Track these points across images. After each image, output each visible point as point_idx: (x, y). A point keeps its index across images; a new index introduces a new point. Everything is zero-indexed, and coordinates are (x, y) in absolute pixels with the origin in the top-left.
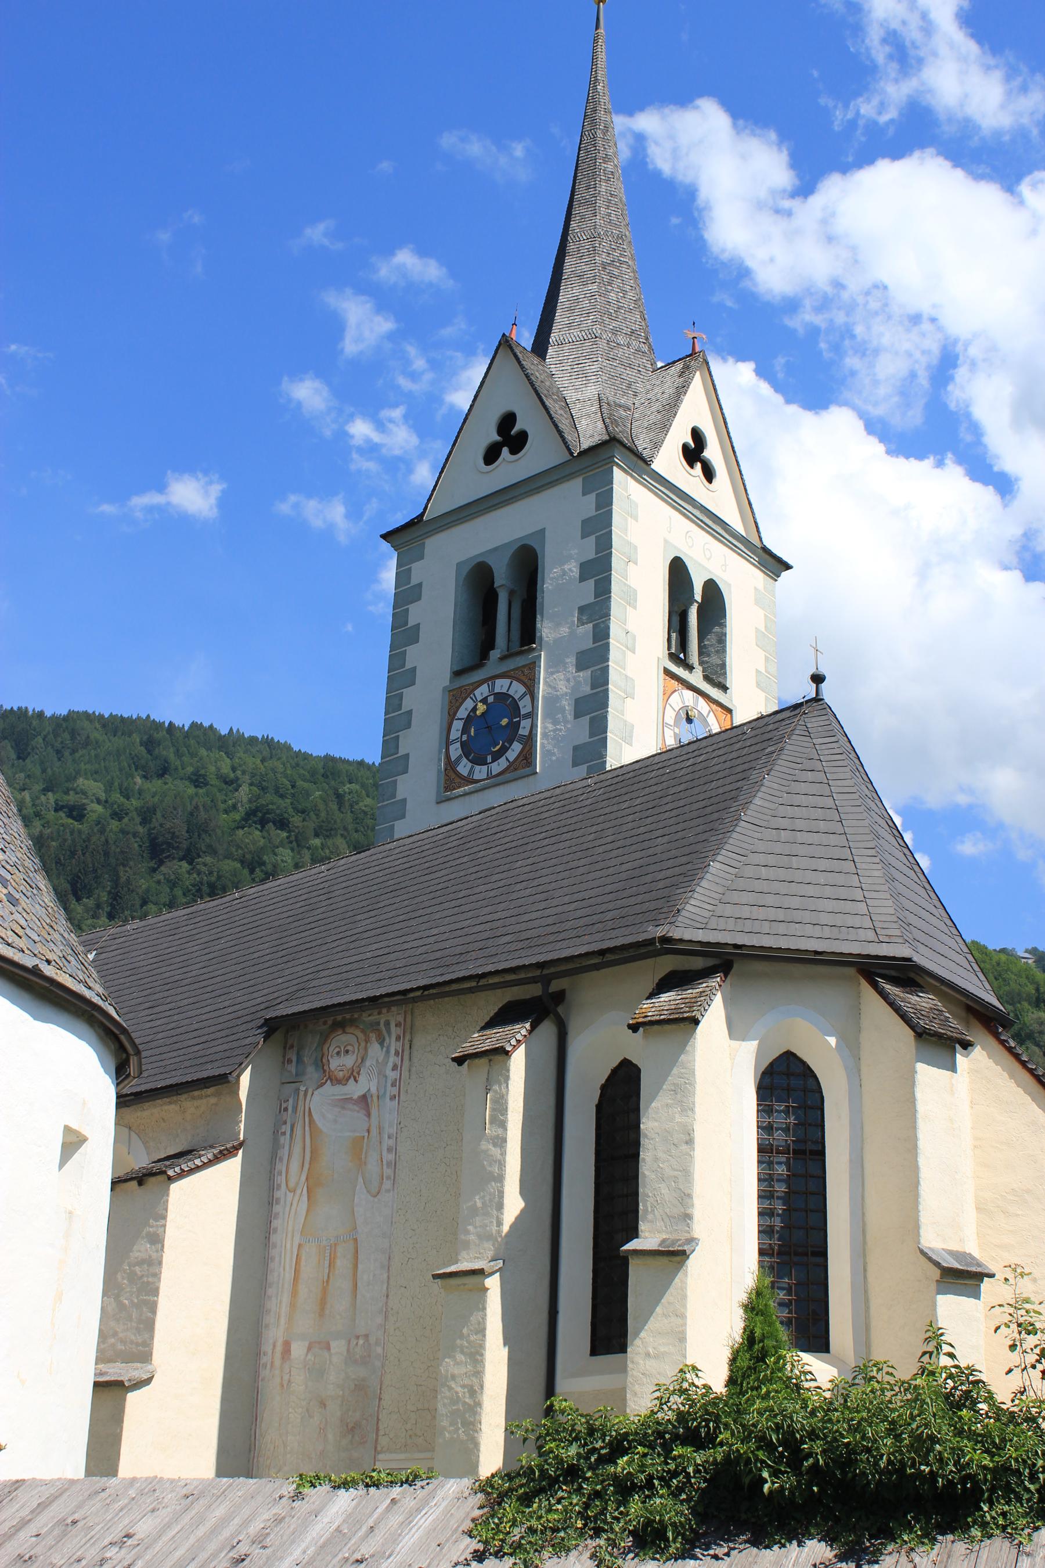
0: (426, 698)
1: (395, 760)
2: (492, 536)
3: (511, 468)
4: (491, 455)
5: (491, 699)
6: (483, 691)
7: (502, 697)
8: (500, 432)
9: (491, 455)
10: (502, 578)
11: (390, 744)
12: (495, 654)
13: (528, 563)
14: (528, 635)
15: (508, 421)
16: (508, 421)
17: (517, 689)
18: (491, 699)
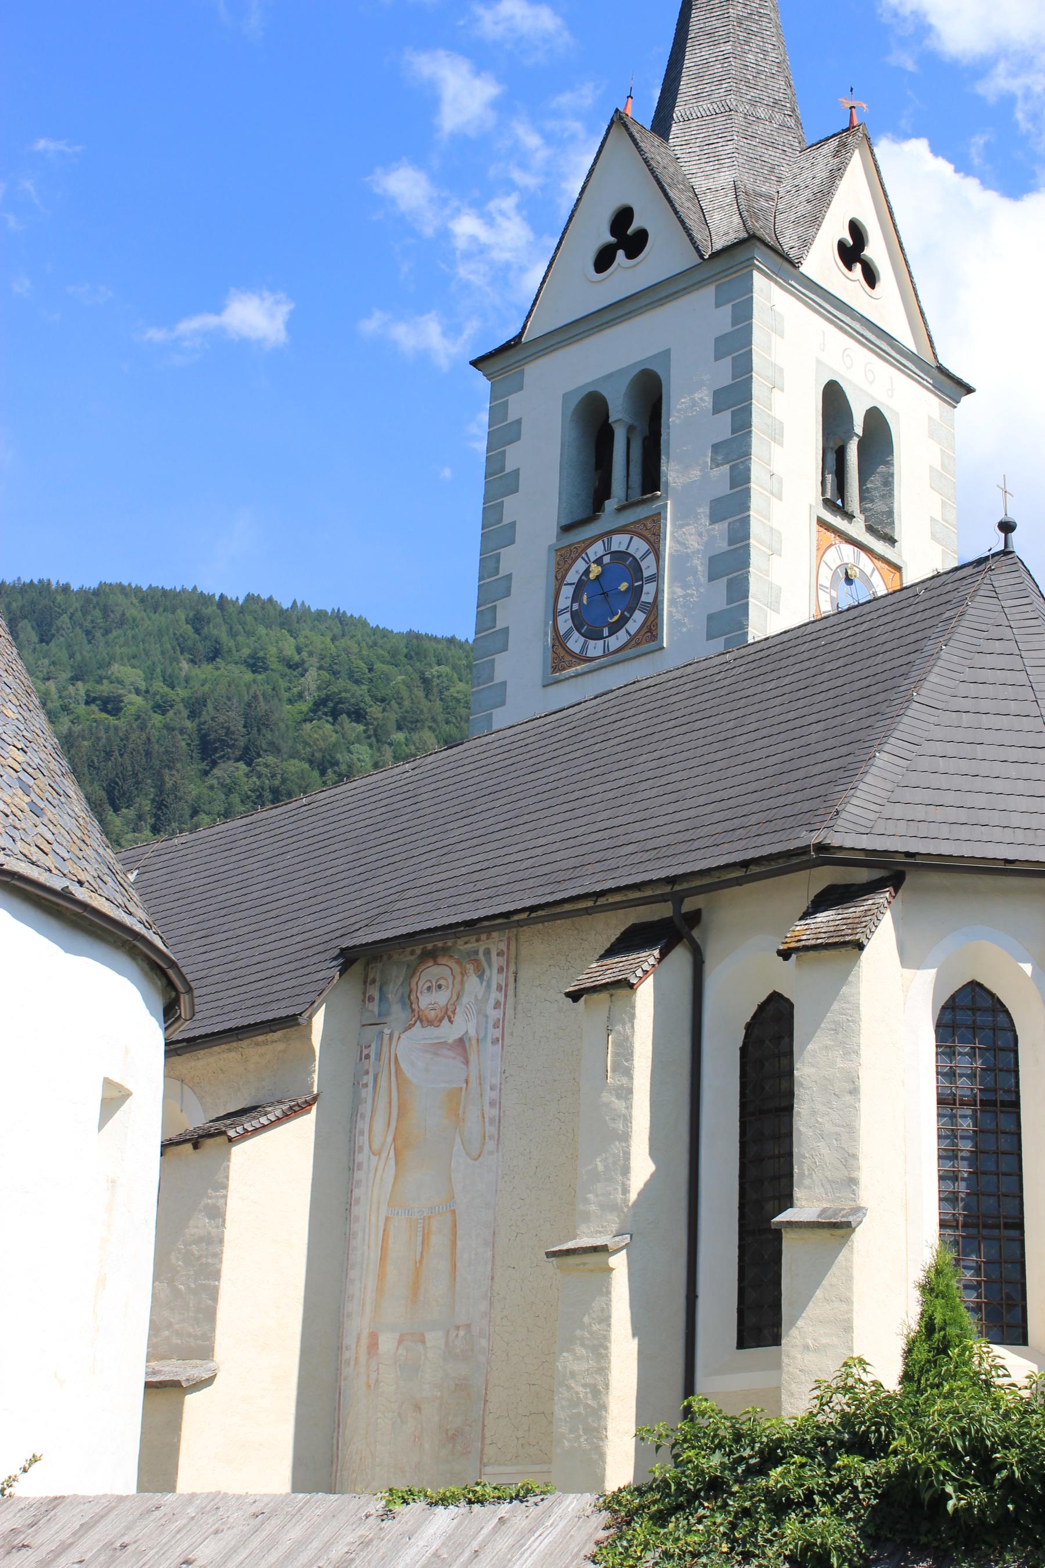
0: (530, 558)
1: (491, 635)
2: (603, 362)
3: (628, 275)
4: (603, 261)
5: (607, 559)
6: (597, 549)
7: (620, 556)
8: (613, 233)
9: (603, 261)
10: (619, 411)
11: (486, 615)
12: (611, 505)
13: (649, 393)
14: (651, 480)
15: (623, 217)
16: (623, 217)
17: (638, 547)
18: (607, 559)
